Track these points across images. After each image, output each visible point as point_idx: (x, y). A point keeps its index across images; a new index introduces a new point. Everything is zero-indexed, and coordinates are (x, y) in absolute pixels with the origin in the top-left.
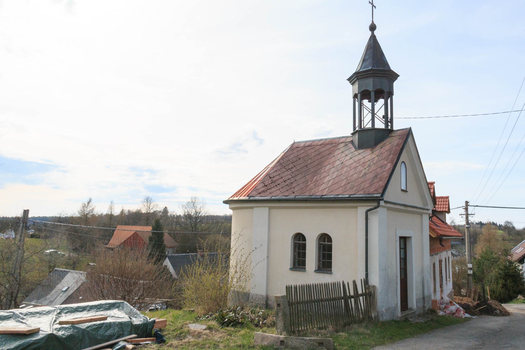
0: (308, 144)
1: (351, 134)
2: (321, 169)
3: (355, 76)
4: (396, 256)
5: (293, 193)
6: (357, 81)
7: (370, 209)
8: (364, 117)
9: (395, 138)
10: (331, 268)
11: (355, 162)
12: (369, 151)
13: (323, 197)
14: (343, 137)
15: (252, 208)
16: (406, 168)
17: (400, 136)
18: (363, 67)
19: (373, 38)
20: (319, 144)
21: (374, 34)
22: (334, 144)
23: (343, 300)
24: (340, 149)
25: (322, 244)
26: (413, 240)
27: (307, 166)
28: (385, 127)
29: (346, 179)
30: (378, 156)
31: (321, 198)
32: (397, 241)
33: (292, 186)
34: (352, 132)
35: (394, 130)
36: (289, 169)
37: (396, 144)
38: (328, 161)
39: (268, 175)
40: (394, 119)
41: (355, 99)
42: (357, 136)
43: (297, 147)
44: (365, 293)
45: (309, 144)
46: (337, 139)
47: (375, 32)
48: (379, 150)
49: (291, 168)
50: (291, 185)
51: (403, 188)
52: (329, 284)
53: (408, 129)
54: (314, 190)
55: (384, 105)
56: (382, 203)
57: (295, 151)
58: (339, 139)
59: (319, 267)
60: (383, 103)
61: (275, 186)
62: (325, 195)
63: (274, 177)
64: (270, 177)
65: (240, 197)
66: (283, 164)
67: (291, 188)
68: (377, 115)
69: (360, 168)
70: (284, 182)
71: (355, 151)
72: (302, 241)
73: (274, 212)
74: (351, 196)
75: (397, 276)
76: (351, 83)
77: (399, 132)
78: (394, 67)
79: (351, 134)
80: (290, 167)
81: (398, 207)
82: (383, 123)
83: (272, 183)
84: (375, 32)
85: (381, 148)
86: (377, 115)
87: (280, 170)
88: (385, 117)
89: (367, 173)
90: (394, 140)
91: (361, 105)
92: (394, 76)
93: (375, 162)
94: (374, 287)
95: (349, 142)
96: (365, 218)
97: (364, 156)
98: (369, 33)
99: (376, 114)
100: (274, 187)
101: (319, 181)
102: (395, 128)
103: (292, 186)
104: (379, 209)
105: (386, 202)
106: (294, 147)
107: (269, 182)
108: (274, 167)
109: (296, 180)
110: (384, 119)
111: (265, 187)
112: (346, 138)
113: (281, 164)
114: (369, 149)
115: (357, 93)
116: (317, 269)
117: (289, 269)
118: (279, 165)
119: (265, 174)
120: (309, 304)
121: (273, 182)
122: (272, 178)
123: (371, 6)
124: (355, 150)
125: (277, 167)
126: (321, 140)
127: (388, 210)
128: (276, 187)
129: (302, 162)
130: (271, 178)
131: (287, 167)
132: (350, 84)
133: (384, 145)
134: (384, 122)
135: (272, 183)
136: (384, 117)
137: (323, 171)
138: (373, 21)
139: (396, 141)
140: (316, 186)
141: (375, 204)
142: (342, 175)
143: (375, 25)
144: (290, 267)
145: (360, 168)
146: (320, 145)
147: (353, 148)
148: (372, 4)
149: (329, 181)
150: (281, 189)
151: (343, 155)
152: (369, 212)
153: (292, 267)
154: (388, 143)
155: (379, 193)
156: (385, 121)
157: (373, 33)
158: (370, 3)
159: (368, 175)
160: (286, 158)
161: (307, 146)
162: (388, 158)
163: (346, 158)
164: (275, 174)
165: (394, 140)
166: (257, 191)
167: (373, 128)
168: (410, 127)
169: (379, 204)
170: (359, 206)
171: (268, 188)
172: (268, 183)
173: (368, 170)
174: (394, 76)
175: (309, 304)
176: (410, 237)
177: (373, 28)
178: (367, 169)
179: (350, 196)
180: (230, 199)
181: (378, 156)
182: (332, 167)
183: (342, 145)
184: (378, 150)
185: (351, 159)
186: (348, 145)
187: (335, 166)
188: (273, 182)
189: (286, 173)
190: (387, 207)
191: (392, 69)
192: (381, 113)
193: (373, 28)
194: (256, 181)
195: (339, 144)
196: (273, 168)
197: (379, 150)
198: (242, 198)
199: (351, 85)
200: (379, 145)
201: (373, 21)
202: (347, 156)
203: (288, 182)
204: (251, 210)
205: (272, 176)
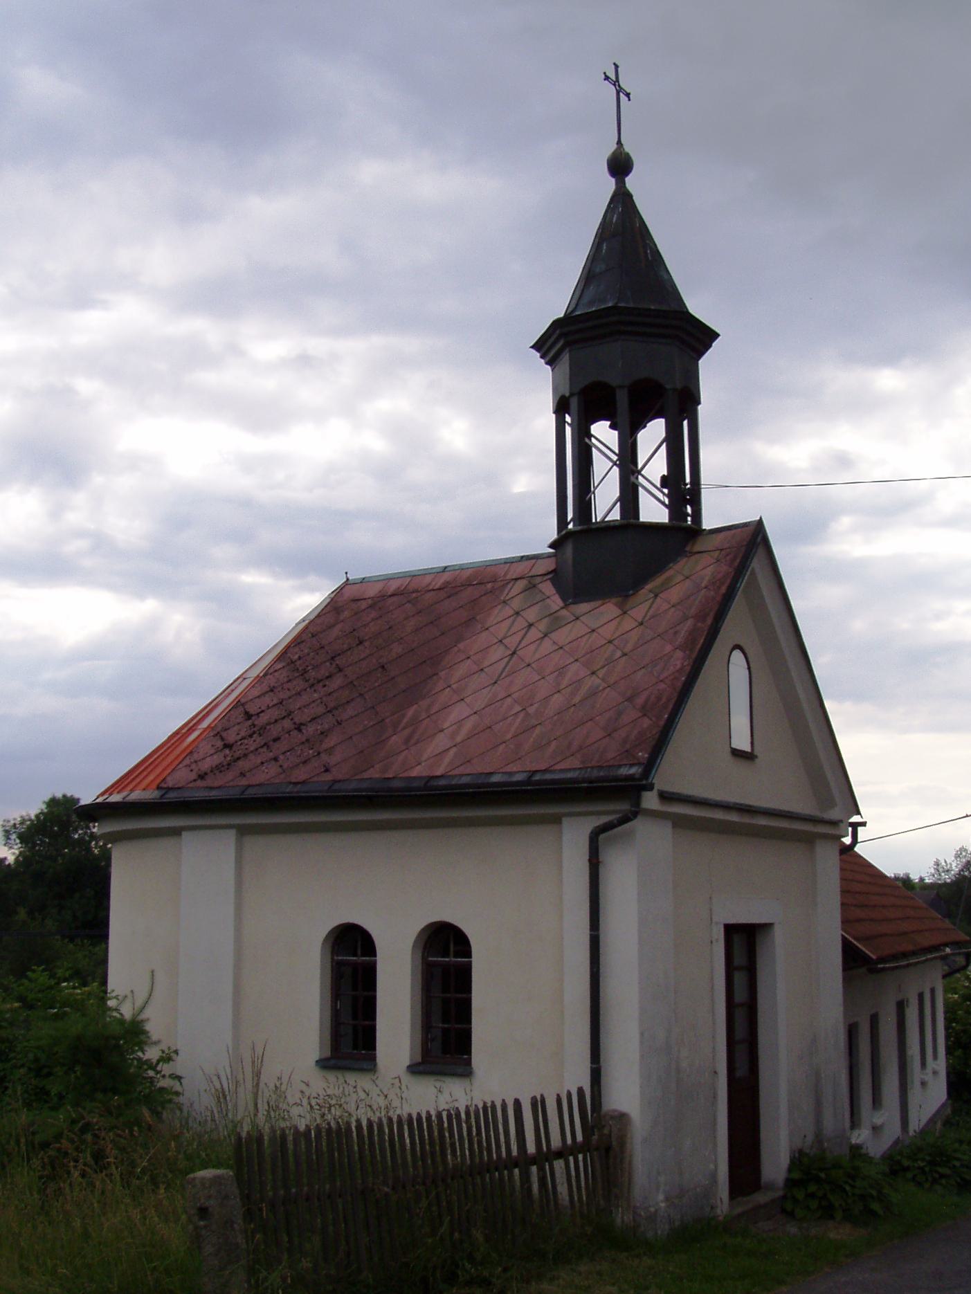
0: (393, 586)
1: (551, 546)
2: (435, 677)
3: (558, 332)
4: (713, 1000)
5: (327, 770)
6: (567, 350)
7: (606, 823)
8: (596, 485)
9: (705, 560)
10: (469, 1052)
11: (561, 648)
12: (609, 609)
13: (434, 783)
14: (522, 557)
15: (176, 832)
16: (749, 668)
17: (721, 550)
18: (585, 300)
19: (622, 202)
20: (437, 587)
21: (627, 185)
22: (489, 585)
23: (516, 1171)
24: (509, 602)
25: (435, 964)
26: (779, 935)
27: (386, 666)
28: (670, 519)
29: (522, 715)
30: (641, 624)
31: (528, 782)
32: (717, 940)
33: (325, 746)
34: (554, 536)
35: (705, 530)
36: (319, 681)
37: (707, 578)
38: (461, 646)
39: (238, 704)
40: (703, 491)
41: (565, 417)
42: (569, 549)
43: (356, 600)
44: (584, 1141)
45: (402, 585)
46: (502, 566)
47: (627, 179)
48: (648, 604)
49: (327, 677)
50: (321, 741)
51: (741, 741)
52: (569, 1095)
53: (752, 528)
54: (401, 757)
55: (664, 445)
56: (650, 801)
57: (346, 613)
58: (509, 567)
59: (426, 1052)
60: (662, 434)
61: (262, 747)
62: (442, 776)
63: (263, 711)
64: (246, 713)
65: (132, 790)
66: (298, 663)
67: (319, 754)
68: (643, 476)
69: (575, 671)
70: (296, 731)
71: (562, 608)
72: (363, 955)
73: (256, 845)
74: (537, 777)
75: (715, 1072)
76: (547, 359)
77: (722, 535)
78: (698, 305)
79: (551, 546)
80: (324, 672)
81: (719, 815)
82: (663, 503)
83: (251, 736)
84: (631, 182)
85: (656, 596)
86: (643, 476)
87: (286, 686)
88: (672, 481)
89: (601, 688)
90: (699, 568)
91: (583, 435)
92: (703, 337)
93: (629, 647)
94: (622, 1118)
95: (545, 575)
96: (590, 860)
97: (594, 626)
98: (610, 184)
99: (639, 472)
100: (257, 749)
101: (425, 722)
102: (708, 523)
103: (325, 746)
104: (640, 826)
105: (665, 797)
106: (345, 598)
107: (243, 734)
108: (265, 675)
109: (339, 723)
110: (666, 491)
111: (227, 751)
112: (534, 561)
113: (292, 662)
114: (614, 600)
115: (567, 394)
116: (420, 1060)
117: (314, 1063)
118: (284, 667)
119: (230, 704)
120: (506, 1172)
121: (254, 733)
122: (253, 718)
123: (613, 90)
124: (562, 604)
125: (276, 674)
126: (443, 571)
127: (675, 825)
128: (265, 749)
129: (368, 652)
130: (248, 716)
131: (312, 674)
132: (543, 361)
133: (665, 586)
134: (667, 501)
135: (251, 736)
136: (665, 481)
137: (441, 685)
138: (619, 142)
139: (709, 571)
140: (413, 741)
141: (624, 807)
142: (509, 700)
143: (628, 155)
144: (318, 1053)
145: (575, 671)
146: (440, 589)
147: (557, 596)
148: (614, 85)
149: (460, 723)
150: (281, 757)
151: (520, 623)
152: (602, 837)
153: (324, 1056)
154: (680, 578)
155: (636, 761)
156: (668, 496)
157: (621, 185)
158: (607, 78)
159: (604, 695)
160: (314, 639)
161: (390, 596)
162: (676, 633)
163: (596, 627)
164: (267, 700)
165: (699, 568)
166: (193, 766)
167: (625, 522)
168: (758, 518)
169: (637, 802)
170: (570, 815)
171: (237, 754)
172: (240, 737)
173: (603, 680)
174: (703, 337)
175: (506, 1172)
176: (767, 927)
177: (620, 166)
178: (601, 673)
179: (530, 777)
180: (98, 801)
181: (641, 624)
182: (475, 668)
183: (521, 585)
184: (641, 607)
185: (546, 638)
186: (540, 586)
187: (486, 663)
188: (254, 733)
189: (305, 698)
190: (669, 814)
191: (691, 311)
192: (655, 467)
193: (620, 166)
194: (194, 731)
195: (507, 583)
196: (260, 679)
197: (648, 604)
198: (136, 795)
199: (548, 367)
200: (649, 586)
201: (619, 142)
202: (533, 627)
203: (310, 730)
204: (167, 843)
205: (252, 709)
